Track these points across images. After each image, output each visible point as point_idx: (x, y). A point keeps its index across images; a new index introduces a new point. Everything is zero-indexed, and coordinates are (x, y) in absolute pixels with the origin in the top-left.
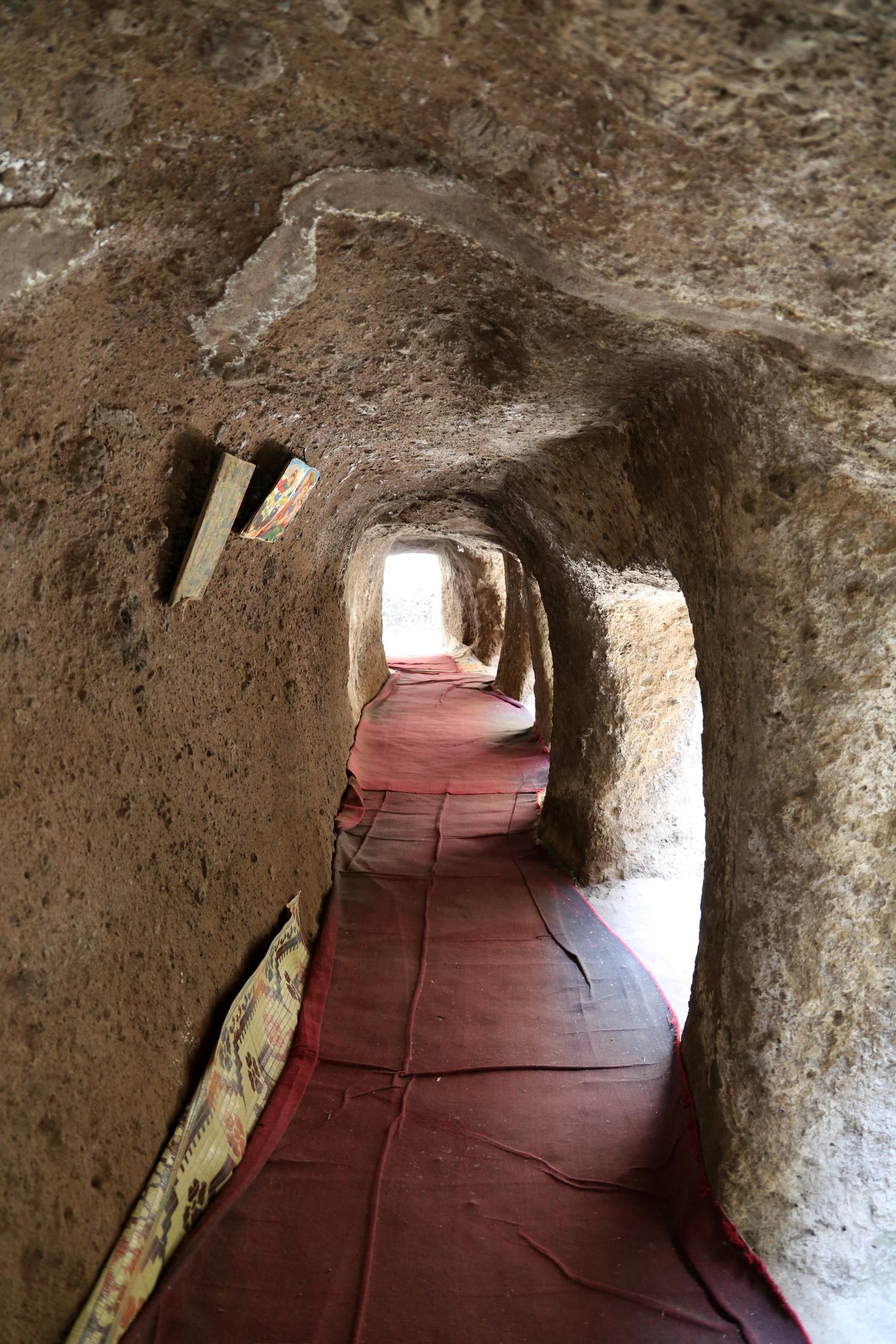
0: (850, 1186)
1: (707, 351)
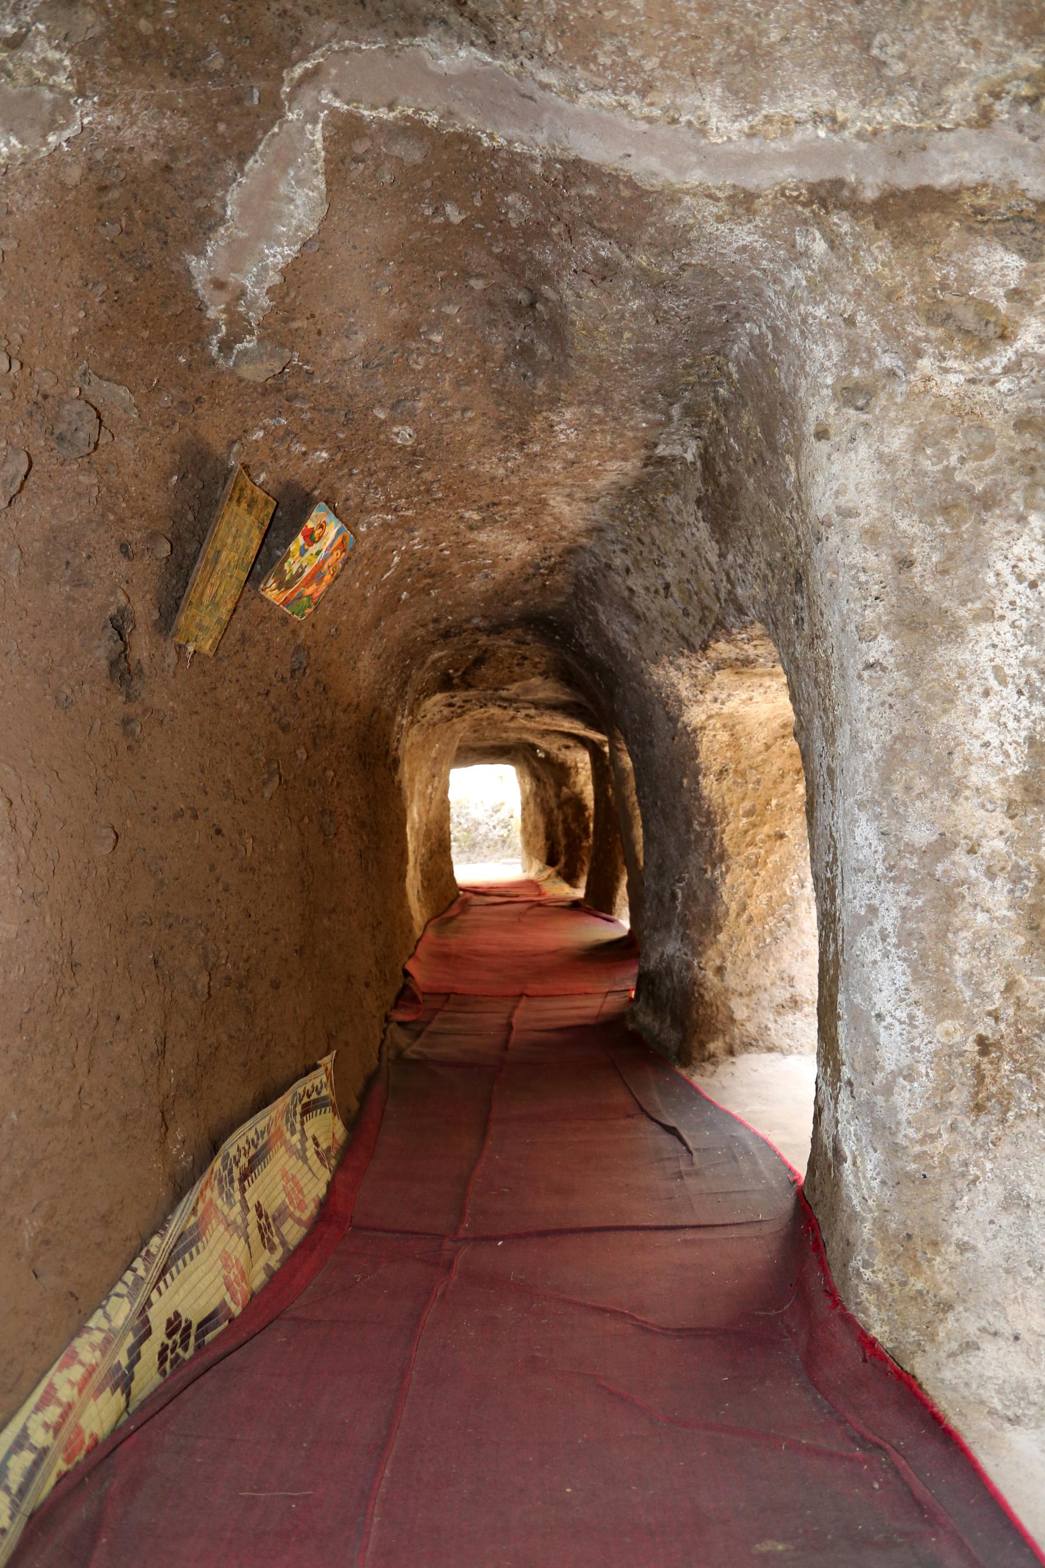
0: (1019, 1279)
1: (757, 245)
